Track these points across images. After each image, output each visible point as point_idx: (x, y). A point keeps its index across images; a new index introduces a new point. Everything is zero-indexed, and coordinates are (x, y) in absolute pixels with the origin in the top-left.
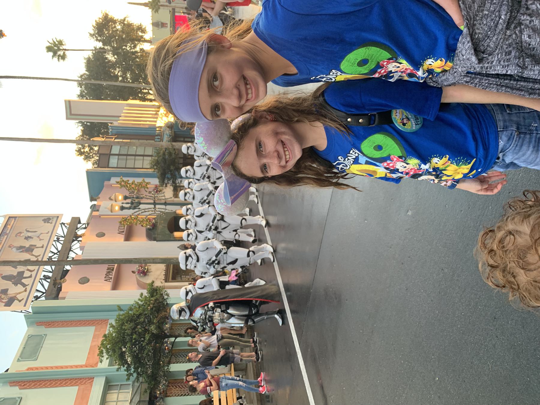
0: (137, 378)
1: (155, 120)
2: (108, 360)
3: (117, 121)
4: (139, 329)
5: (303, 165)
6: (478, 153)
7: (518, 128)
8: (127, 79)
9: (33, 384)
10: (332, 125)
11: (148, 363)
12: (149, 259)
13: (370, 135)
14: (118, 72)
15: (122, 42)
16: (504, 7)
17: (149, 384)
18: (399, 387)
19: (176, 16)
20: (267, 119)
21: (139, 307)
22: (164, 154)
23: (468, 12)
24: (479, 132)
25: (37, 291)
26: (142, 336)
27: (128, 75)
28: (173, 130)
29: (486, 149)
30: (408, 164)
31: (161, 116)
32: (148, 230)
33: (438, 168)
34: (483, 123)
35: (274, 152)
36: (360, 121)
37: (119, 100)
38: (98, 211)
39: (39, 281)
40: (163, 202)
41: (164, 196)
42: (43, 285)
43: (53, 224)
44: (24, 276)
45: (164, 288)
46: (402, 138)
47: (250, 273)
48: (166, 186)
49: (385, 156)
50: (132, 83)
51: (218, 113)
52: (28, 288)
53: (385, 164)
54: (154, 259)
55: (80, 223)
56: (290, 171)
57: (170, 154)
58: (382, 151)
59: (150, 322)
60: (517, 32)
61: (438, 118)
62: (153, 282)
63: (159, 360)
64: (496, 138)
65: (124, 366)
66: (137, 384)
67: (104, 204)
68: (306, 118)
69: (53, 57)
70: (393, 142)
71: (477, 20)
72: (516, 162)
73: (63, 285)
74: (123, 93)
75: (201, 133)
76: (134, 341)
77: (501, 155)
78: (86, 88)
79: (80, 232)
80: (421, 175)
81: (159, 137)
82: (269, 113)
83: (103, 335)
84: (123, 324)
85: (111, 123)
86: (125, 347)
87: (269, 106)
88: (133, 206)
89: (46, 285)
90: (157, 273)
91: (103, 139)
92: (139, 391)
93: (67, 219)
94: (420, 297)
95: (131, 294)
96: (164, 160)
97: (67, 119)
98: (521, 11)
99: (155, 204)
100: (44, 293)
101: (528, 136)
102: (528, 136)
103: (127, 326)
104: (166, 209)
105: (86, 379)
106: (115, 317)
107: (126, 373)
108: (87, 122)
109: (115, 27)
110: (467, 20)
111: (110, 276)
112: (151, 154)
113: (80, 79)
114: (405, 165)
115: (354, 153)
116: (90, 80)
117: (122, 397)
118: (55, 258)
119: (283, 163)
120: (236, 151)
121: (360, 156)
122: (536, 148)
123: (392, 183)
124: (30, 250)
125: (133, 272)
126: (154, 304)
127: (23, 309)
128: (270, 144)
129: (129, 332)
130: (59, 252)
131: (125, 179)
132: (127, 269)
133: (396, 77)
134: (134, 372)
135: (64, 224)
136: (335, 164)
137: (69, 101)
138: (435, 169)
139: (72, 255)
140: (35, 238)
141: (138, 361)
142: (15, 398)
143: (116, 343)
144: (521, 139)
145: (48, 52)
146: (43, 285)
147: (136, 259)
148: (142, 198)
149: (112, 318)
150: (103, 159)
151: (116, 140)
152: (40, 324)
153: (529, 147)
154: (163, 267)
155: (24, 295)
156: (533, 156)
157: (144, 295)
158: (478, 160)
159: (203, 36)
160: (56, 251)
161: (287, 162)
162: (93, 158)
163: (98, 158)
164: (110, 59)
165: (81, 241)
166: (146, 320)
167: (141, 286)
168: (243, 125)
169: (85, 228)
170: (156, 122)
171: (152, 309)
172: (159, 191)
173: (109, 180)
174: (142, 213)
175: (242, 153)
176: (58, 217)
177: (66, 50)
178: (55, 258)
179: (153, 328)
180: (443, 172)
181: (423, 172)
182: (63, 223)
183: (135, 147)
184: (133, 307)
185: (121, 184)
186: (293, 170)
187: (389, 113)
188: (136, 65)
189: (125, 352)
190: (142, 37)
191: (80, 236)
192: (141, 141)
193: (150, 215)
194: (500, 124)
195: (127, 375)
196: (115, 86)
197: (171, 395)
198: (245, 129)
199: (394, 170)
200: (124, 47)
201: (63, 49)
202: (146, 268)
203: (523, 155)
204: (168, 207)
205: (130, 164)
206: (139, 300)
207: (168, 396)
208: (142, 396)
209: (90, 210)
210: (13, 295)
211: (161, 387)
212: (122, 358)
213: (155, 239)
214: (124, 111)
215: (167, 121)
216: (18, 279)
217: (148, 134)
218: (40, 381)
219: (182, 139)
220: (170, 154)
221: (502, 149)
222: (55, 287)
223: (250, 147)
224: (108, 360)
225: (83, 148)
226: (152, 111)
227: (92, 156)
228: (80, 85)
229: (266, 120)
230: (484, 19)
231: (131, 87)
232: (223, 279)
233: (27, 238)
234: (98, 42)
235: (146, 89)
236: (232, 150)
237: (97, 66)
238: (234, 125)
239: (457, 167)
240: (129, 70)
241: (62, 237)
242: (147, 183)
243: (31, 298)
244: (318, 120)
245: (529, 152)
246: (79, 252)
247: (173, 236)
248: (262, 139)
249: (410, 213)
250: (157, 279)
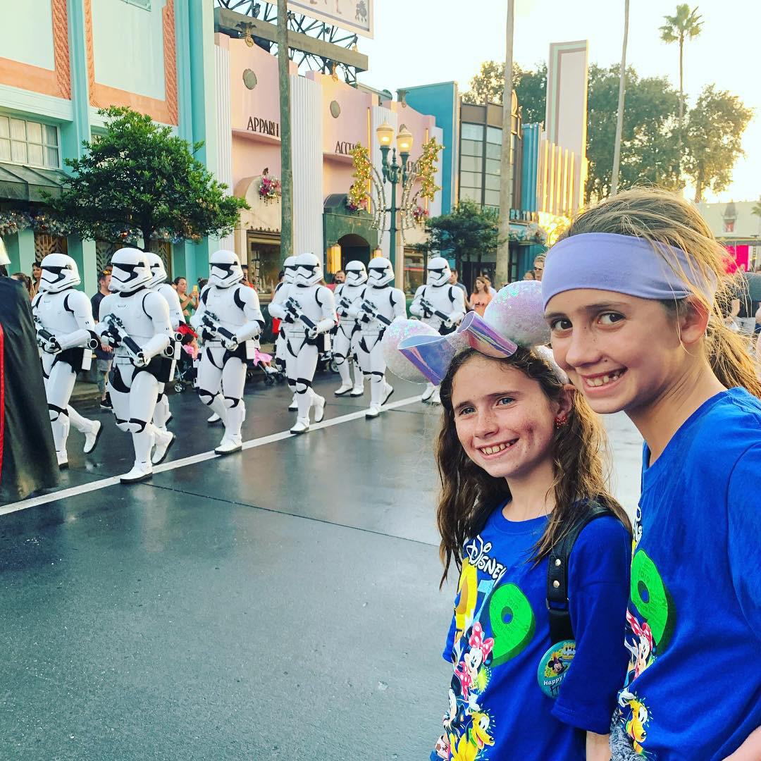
0: (69, 180)
1: (551, 210)
2: (103, 126)
4: (161, 183)
5: (475, 479)
8: (627, 156)
11: (96, 200)
13: (530, 599)
14: (640, 140)
17: (59, 201)
18: (56, 665)
20: (559, 412)
21: (201, 183)
22: (487, 227)
27: (634, 159)
28: (531, 243)
30: (479, 669)
31: (558, 220)
32: (344, 199)
33: (472, 727)
35: (496, 425)
36: (557, 583)
37: (588, 141)
38: (380, 104)
40: (398, 226)
41: (408, 228)
43: (357, 22)
47: (265, 389)
48: (426, 231)
50: (621, 165)
51: (559, 325)
53: (478, 628)
55: (358, 70)
56: (466, 456)
57: (487, 238)
58: (501, 621)
59: (172, 203)
62: (248, 208)
65: (91, 154)
66: (58, 179)
67: (393, 115)
68: (562, 483)
69: (668, 17)
75: (526, 293)
76: (139, 172)
78: (609, 79)
79: (339, 70)
80: (457, 693)
81: (518, 218)
83: (151, 116)
84: (169, 152)
85: (544, 127)
86: (126, 157)
87: (583, 416)
88: (389, 169)
90: (263, 215)
92: (45, 183)
93: (363, 47)
94: (224, 706)
95: (225, 167)
96: (477, 227)
97: (552, 45)
103: (166, 160)
105: (69, 84)
106: (182, 138)
107: (80, 159)
108: (546, 82)
109: (726, 133)
111: (258, 128)
113: (627, 68)
114: (477, 665)
115: (497, 570)
116: (626, 88)
117: (36, 152)
118: (292, 26)
119: (478, 443)
120: (496, 356)
123: (444, 646)
126: (207, 209)
128: (510, 418)
129: (155, 163)
130: (303, 32)
131: (439, 155)
132: (271, 159)
133: (633, 650)
134: (81, 173)
135: (355, 41)
136: (478, 537)
137: (584, 49)
138: (469, 719)
141: (101, 181)
143: (135, 140)
145: (678, 8)
147: (291, 176)
149: (180, 132)
150: (478, 114)
151: (512, 136)
154: (276, 226)
157: (224, 191)
159: (707, 293)
160: (304, 26)
161: (480, 449)
162: (479, 94)
165: (323, 73)
166: (177, 196)
167: (241, 185)
168: (546, 367)
169: (348, 81)
170: (547, 211)
171: (198, 205)
172: (416, 218)
174: (377, 186)
175: (494, 366)
176: (368, 30)
177: (682, 41)
179: (164, 207)
180: (464, 735)
182: (356, 38)
184: (200, 171)
185: (430, 146)
189: (117, 156)
190: (708, 184)
191: (331, 72)
192: (511, 183)
195: (76, 161)
196: (615, 133)
197: (39, 242)
198: (537, 371)
199: (468, 644)
200: (687, 150)
201: (682, 37)
202: (274, 195)
204: (387, 235)
205: (467, 163)
207: (36, 238)
208: (36, 189)
211: (54, 224)
212: (107, 150)
213: (327, 211)
214: (567, 151)
215: (548, 232)
217: (522, 197)
219: (514, 261)
220: (487, 238)
222: (238, 25)
223: (506, 380)
224: (103, 126)
227: (483, 93)
228: (615, 70)
229: (557, 410)
232: (88, 356)
234: (697, 101)
237: (649, 103)
238: (546, 353)
240: (644, 159)
241: (331, 39)
242: (432, 196)
244: (559, 504)
246: (303, 70)
247: (334, 245)
248: (520, 403)
249: (381, 687)
250: (253, 214)
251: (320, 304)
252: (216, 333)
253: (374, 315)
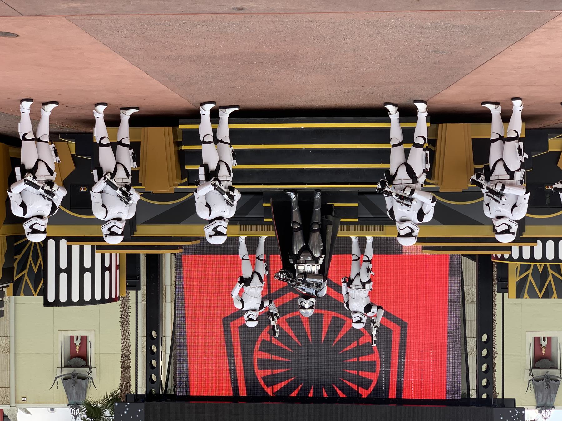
137: (127, 286)
251: (104, 206)
252: (226, 190)
253: (43, 188)
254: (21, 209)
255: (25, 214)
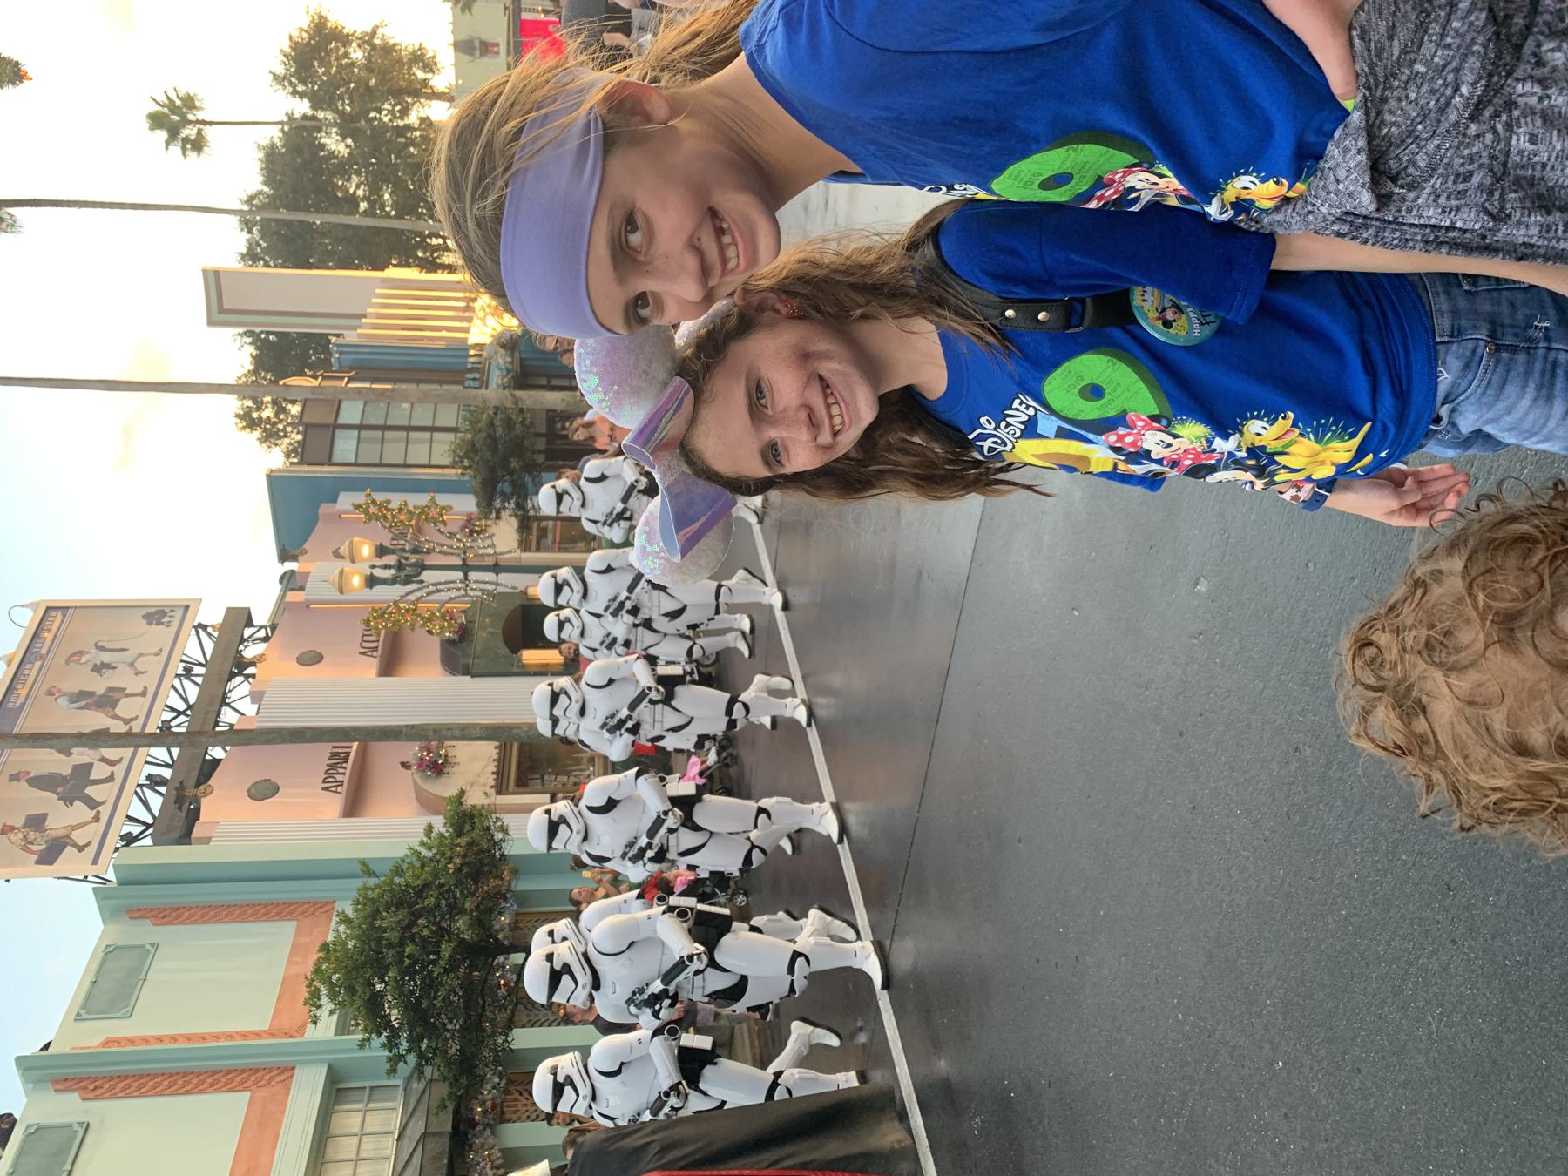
0: (419, 1069)
1: (465, 325)
2: (335, 1017)
3: (355, 328)
6: (1379, 407)
7: (1493, 335)
8: (383, 206)
9: (121, 1085)
10: (963, 328)
11: (450, 1027)
12: (449, 727)
14: (358, 187)
15: (368, 97)
16: (1472, 60)
19: (524, 22)
20: (778, 312)
21: (423, 866)
22: (491, 424)
23: (1371, 66)
24: (1383, 345)
25: (130, 819)
26: (431, 948)
27: (387, 196)
28: (517, 355)
29: (1402, 395)
30: (1175, 436)
31: (481, 314)
33: (1263, 447)
34: (1389, 313)
35: (797, 409)
36: (1042, 316)
38: (302, 588)
39: (134, 791)
40: (489, 562)
41: (493, 546)
42: (145, 803)
43: (174, 628)
44: (93, 777)
45: (493, 809)
46: (1159, 364)
47: (742, 766)
48: (498, 518)
49: (1112, 413)
50: (395, 217)
51: (644, 313)
52: (105, 811)
53: (1113, 438)
54: (463, 727)
55: (249, 623)
56: (846, 456)
57: (509, 424)
59: (455, 909)
60: (1499, 126)
61: (1266, 310)
62: (462, 793)
63: (481, 1016)
64: (1430, 363)
65: (380, 1035)
66: (417, 1086)
67: (319, 569)
69: (168, 143)
70: (1135, 377)
71: (1391, 88)
72: (1488, 429)
73: (205, 802)
74: (373, 249)
75: (593, 364)
76: (407, 961)
77: (1444, 411)
78: (263, 234)
79: (250, 652)
80: (1213, 469)
82: (784, 297)
84: (376, 914)
85: (338, 336)
86: (383, 981)
88: (403, 575)
89: (156, 802)
90: (474, 768)
91: (315, 383)
93: (212, 614)
95: (397, 829)
96: (492, 438)
97: (211, 323)
98: (1519, 73)
99: (465, 568)
100: (148, 826)
101: (1522, 357)
102: (1522, 357)
103: (389, 920)
104: (498, 584)
105: (271, 1070)
106: (354, 894)
107: (386, 1053)
108: (268, 333)
109: (346, 55)
110: (1369, 88)
111: (339, 778)
112: (453, 425)
113: (246, 208)
115: (1022, 408)
116: (277, 208)
117: (374, 1121)
118: (181, 725)
119: (825, 437)
120: (691, 408)
121: (1040, 416)
122: (1544, 392)
124: (107, 701)
125: (405, 765)
126: (464, 856)
127: (91, 871)
128: (786, 388)
129: (393, 936)
130: (190, 707)
131: (380, 497)
132: (388, 756)
134: (409, 1050)
135: (204, 627)
137: (217, 273)
138: (1253, 452)
139: (228, 717)
140: (122, 668)
141: (421, 1019)
142: (70, 1126)
143: (357, 968)
144: (1500, 369)
145: (152, 128)
146: (145, 803)
147: (413, 727)
148: (428, 552)
149: (344, 898)
150: (316, 440)
152: (138, 913)
153: (1525, 386)
154: (489, 749)
155: (91, 833)
156: (1537, 413)
158: (1379, 425)
159: (598, 81)
160: (181, 706)
161: (835, 434)
162: (286, 436)
163: (299, 437)
164: (333, 147)
165: (254, 676)
166: (443, 902)
167: (427, 803)
169: (266, 639)
171: (459, 870)
172: (479, 533)
173: (334, 500)
174: (429, 594)
175: (707, 413)
176: (187, 607)
177: (204, 123)
178: (181, 725)
179: (461, 923)
180: (1277, 458)
181: (1219, 461)
182: (200, 625)
183: (406, 406)
184: (404, 866)
185: (366, 512)
186: (853, 455)
187: (1125, 296)
188: (410, 165)
189: (381, 994)
190: (425, 82)
191: (252, 663)
193: (451, 600)
194: (1442, 324)
195: (390, 1059)
196: (346, 226)
197: (515, 1117)
198: (715, 344)
200: (372, 114)
201: (198, 122)
202: (443, 752)
203: (1509, 411)
204: (504, 578)
205: (394, 453)
206: (422, 844)
207: (509, 1121)
208: (433, 1119)
209: (279, 587)
210: (62, 832)
211: (487, 1093)
212: (374, 1006)
213: (466, 671)
215: (499, 329)
216: (73, 787)
217: (444, 367)
218: (141, 1077)
219: (544, 382)
221: (1447, 396)
222: (180, 808)
223: (730, 397)
224: (335, 1017)
225: (259, 409)
226: (456, 299)
227: (284, 430)
228: (247, 225)
230: (1412, 88)
231: (394, 230)
233: (99, 668)
234: (297, 100)
235: (438, 236)
236: (679, 407)
237: (296, 169)
238: (686, 331)
239: (1317, 447)
240: (387, 181)
241: (200, 664)
242: (443, 508)
243: (113, 840)
244: (920, 312)
245: (1525, 403)
246: (249, 709)
247: (520, 660)
248: (763, 372)
251: (611, 681)
252: (656, 841)
254: (601, 802)
255: (587, 479)
